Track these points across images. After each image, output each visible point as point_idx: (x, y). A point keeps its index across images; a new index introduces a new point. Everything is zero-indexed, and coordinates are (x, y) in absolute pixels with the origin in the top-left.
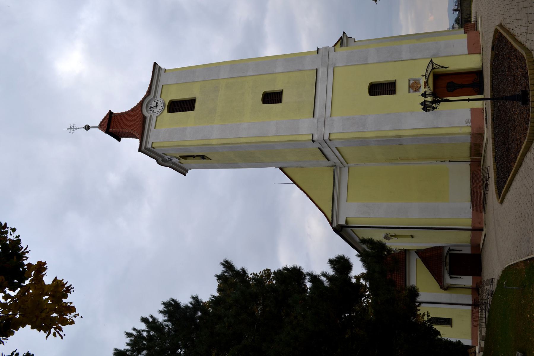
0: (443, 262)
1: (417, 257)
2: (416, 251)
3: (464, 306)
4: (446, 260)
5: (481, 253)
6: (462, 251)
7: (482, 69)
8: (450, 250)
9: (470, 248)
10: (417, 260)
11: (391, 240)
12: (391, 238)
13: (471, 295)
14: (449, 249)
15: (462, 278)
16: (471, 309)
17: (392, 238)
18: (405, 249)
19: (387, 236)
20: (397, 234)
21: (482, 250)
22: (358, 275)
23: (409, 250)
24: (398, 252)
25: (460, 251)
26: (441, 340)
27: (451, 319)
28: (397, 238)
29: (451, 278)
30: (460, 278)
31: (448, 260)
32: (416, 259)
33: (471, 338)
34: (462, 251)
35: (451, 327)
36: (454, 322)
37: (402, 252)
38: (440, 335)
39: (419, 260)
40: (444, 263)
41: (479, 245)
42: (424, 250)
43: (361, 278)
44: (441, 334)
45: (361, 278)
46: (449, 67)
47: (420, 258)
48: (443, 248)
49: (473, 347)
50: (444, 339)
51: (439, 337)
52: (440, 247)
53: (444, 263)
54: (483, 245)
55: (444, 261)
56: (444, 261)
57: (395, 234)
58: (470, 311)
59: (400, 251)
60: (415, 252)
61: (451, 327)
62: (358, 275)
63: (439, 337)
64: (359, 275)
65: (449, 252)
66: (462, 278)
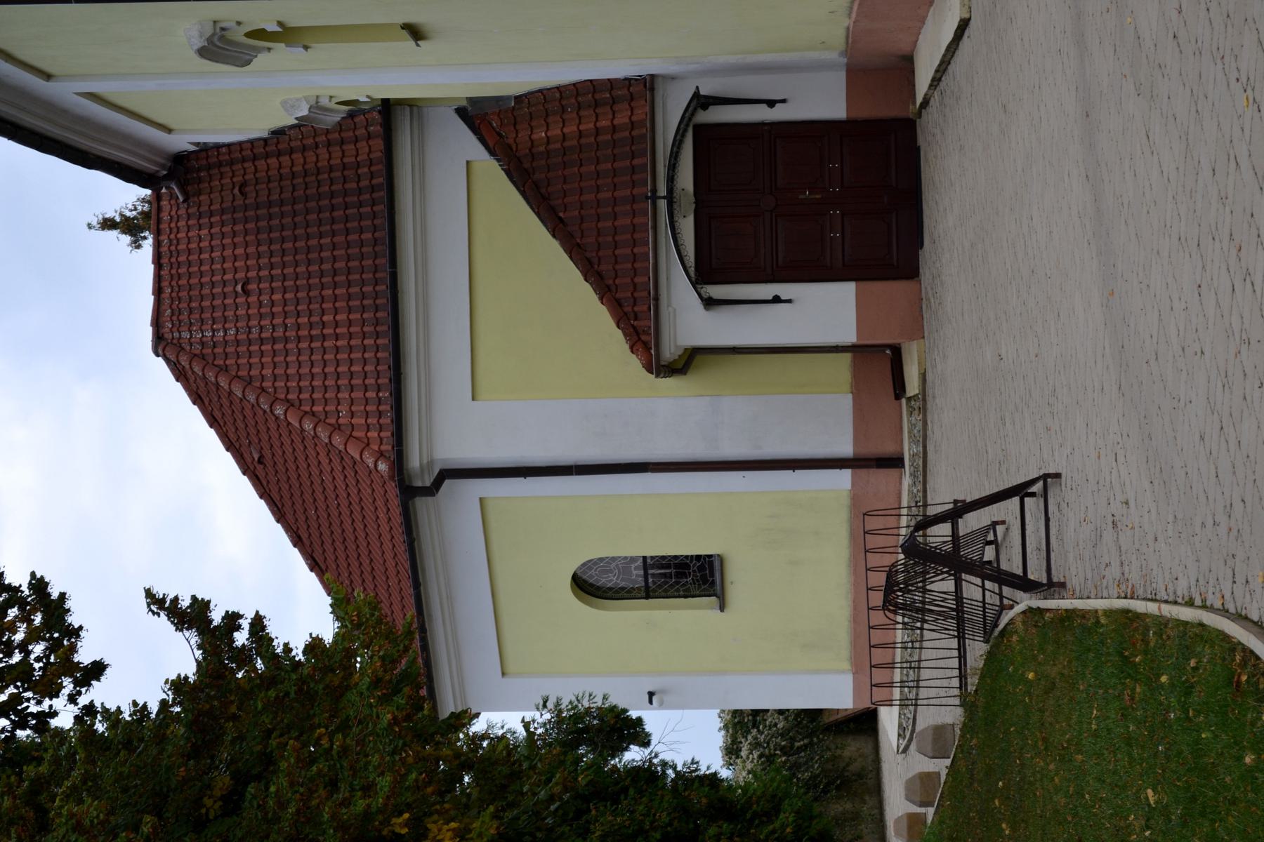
0: (655, 198)
1: (477, 151)
2: (464, 103)
3: (800, 474)
4: (671, 180)
5: (920, 115)
6: (783, 101)
7: (350, 441)
8: (701, 101)
9: (842, 76)
10: (476, 167)
11: (261, 61)
12: (258, 50)
13: (850, 396)
14: (697, 95)
15: (789, 301)
16: (849, 487)
17: (269, 49)
18: (386, 102)
19: (222, 38)
20: (293, 22)
21: (926, 103)
22: (122, 215)
23: (411, 105)
24: (337, 118)
25: (771, 103)
26: (648, 775)
27: (721, 558)
28: (306, 48)
29: (709, 303)
30: (777, 300)
31: (686, 179)
32: (468, 162)
33: (846, 665)
34: (783, 101)
35: (722, 608)
36: (737, 579)
37: (360, 119)
38: (644, 741)
39: (491, 171)
40: (663, 204)
41: (907, 63)
42: (518, 99)
43: (147, 234)
44: (648, 735)
45: (147, 234)
46: (545, 694)
47: (492, 152)
48: (652, 89)
49: (865, 722)
50: (674, 767)
51: (634, 755)
52: (628, 82)
53: (663, 204)
54: (936, 82)
55: (662, 190)
56: (662, 190)
57: (280, 24)
58: (845, 500)
59: (351, 115)
60: (461, 112)
61: (722, 608)
62: (122, 215)
63: (634, 755)
64: (128, 214)
65: (693, 114)
66: (789, 301)
